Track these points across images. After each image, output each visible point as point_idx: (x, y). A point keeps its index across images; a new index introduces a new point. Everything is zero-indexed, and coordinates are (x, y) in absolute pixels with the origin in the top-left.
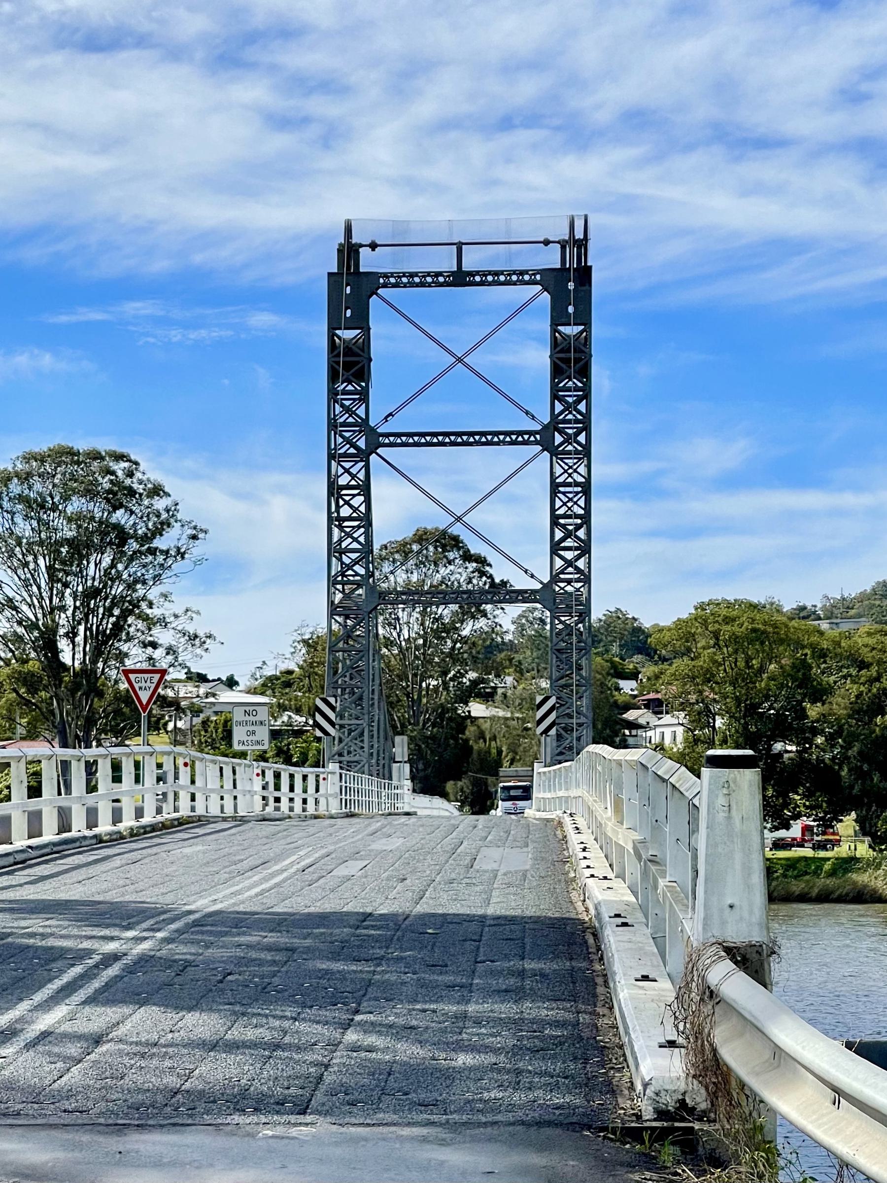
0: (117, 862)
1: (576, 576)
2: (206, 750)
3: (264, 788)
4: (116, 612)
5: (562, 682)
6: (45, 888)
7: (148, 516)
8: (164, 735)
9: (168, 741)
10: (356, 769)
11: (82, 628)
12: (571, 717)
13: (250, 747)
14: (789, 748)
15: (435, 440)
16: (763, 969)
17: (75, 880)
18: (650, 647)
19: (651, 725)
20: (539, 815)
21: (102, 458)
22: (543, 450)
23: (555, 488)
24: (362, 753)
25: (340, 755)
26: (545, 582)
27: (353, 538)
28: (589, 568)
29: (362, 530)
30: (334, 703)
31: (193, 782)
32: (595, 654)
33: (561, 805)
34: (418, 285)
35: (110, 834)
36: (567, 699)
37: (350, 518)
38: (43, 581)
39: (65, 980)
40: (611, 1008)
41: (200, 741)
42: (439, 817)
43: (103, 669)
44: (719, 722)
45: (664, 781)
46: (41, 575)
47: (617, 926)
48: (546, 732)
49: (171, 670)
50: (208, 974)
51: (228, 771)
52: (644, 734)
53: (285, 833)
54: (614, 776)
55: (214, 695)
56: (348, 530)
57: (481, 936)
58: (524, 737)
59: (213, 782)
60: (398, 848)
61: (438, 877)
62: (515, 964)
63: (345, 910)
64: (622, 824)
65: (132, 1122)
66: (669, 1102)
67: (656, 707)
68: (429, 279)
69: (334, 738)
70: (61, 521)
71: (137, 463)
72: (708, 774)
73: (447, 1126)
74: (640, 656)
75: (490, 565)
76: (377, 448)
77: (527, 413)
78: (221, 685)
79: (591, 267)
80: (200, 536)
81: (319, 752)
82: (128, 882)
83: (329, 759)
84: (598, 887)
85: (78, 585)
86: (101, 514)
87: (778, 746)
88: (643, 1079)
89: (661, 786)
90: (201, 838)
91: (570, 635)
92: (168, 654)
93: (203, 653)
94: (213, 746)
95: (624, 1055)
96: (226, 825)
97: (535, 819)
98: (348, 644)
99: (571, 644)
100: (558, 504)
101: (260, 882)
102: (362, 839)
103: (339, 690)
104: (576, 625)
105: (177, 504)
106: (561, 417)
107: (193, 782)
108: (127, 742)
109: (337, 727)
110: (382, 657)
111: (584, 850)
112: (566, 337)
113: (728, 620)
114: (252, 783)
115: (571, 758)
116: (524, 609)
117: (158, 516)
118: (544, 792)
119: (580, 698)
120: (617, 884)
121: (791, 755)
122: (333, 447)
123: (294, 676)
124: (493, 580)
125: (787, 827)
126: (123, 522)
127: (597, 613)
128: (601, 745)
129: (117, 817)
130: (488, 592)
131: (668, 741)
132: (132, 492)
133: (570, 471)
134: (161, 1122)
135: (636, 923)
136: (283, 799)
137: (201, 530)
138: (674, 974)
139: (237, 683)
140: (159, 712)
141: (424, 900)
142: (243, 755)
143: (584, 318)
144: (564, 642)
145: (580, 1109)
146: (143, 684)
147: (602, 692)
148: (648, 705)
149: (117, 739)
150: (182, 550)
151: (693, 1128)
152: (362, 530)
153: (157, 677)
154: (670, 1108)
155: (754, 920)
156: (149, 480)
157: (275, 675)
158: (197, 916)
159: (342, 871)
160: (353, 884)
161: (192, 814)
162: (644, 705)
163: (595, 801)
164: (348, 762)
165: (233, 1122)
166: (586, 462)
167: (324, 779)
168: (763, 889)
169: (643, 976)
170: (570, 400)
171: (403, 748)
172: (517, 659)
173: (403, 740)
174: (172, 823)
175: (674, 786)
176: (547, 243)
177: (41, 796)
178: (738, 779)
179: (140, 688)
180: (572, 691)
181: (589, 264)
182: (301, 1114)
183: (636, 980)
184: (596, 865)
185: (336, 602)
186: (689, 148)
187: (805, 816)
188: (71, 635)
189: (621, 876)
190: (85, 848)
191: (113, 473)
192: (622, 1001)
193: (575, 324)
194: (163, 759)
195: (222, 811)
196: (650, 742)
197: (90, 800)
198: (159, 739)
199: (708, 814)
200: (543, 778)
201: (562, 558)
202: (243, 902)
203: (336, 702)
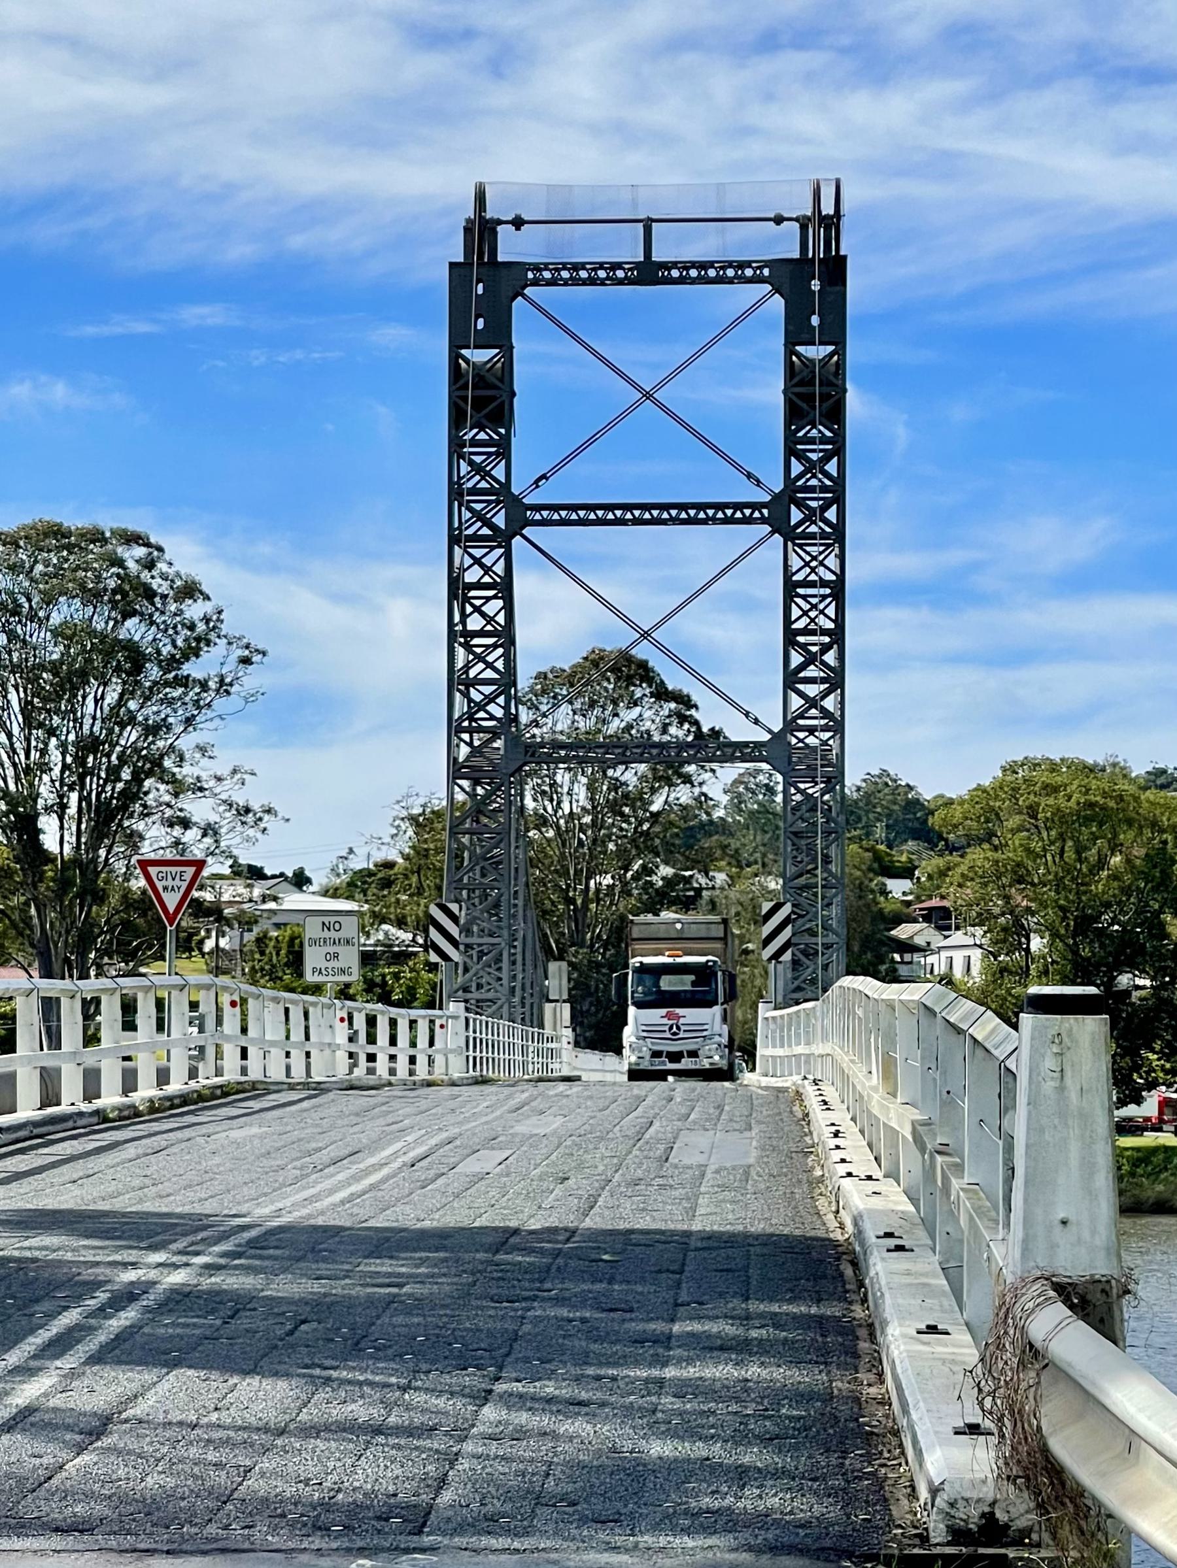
0: (131, 1150)
1: (823, 722)
2: (262, 981)
3: (351, 1040)
4: (126, 774)
5: (802, 881)
6: (22, 1191)
7: (175, 627)
8: (199, 959)
9: (205, 967)
10: (490, 1011)
11: (74, 797)
12: (815, 935)
13: (330, 978)
14: (1140, 982)
15: (610, 516)
16: (1112, 1317)
17: (67, 1178)
18: (932, 830)
19: (933, 946)
20: (766, 1081)
21: (104, 541)
22: (773, 533)
23: (791, 588)
24: (499, 988)
25: (466, 990)
26: (776, 730)
27: (486, 662)
28: (842, 709)
29: (500, 651)
30: (457, 912)
31: (244, 1030)
32: (849, 839)
33: (799, 1067)
34: (584, 283)
35: (120, 1110)
36: (808, 907)
37: (482, 633)
38: (15, 725)
39: (55, 1331)
40: (880, 1376)
41: (253, 968)
42: (614, 1084)
43: (107, 859)
44: (1037, 944)
45: (959, 1031)
46: (13, 717)
47: (889, 1251)
48: (776, 956)
49: (210, 860)
50: (270, 1322)
51: (296, 1015)
52: (922, 960)
53: (384, 1108)
54: (883, 1024)
55: (275, 899)
56: (479, 650)
57: (683, 1265)
58: (743, 965)
59: (274, 1032)
60: (555, 1131)
61: (617, 1175)
62: (736, 1304)
63: (476, 1224)
64: (895, 1096)
65: (159, 1546)
66: (972, 1516)
67: (941, 919)
68: (602, 274)
69: (457, 964)
70: (42, 635)
71: (160, 549)
72: (1031, 1021)
73: (637, 1553)
74: (915, 843)
75: (696, 707)
76: (523, 528)
77: (749, 476)
78: (284, 883)
79: (845, 257)
80: (254, 659)
81: (434, 988)
82: (147, 1181)
83: (449, 997)
84: (859, 1192)
85: (68, 732)
86: (103, 624)
87: (1124, 980)
88: (930, 1483)
89: (953, 1038)
90: (256, 1116)
91: (813, 809)
92: (204, 835)
93: (259, 835)
94: (274, 978)
95: (901, 1445)
96: (294, 1096)
97: (760, 1087)
98: (478, 822)
99: (815, 824)
100: (795, 612)
101: (348, 1182)
102: (501, 1117)
103: (464, 893)
104: (822, 795)
105: (220, 613)
106: (799, 483)
107: (244, 1030)
108: (143, 970)
109: (462, 947)
110: (531, 842)
111: (836, 1135)
112: (808, 363)
113: (1051, 789)
114: (333, 1033)
115: (814, 996)
116: (742, 771)
117: (192, 627)
118: (774, 1046)
119: (829, 905)
120: (888, 1187)
121: (1143, 993)
122: (456, 525)
123: (396, 870)
124: (699, 728)
125: (1138, 1101)
126: (137, 638)
127: (853, 778)
128: (862, 978)
129: (129, 1083)
130: (690, 745)
131: (958, 973)
132: (149, 594)
133: (814, 564)
134: (203, 1547)
135: (917, 1246)
136: (380, 1057)
137: (257, 650)
138: (975, 1322)
139: (308, 881)
140: (191, 923)
141: (596, 1210)
142: (317, 989)
143: (835, 334)
144: (804, 821)
145: (836, 1528)
146: (170, 883)
147: (860, 897)
148: (929, 916)
149: (127, 964)
150: (228, 680)
151: (1006, 1555)
152: (500, 651)
153: (190, 871)
154: (971, 1526)
155: (1098, 1242)
156: (178, 575)
157: (368, 869)
158: (254, 1233)
159: (471, 1166)
160: (488, 1186)
161: (243, 1079)
162: (922, 916)
163: (852, 1061)
164: (478, 1001)
165: (312, 1547)
166: (837, 551)
167: (442, 1026)
168: (1112, 1194)
169: (928, 1327)
170: (814, 456)
171: (560, 980)
172: (733, 846)
173: (560, 967)
174: (212, 1093)
175: (975, 1040)
176: (779, 220)
177: (15, 1052)
178: (1075, 1029)
179: (165, 888)
180: (815, 895)
181: (842, 253)
182: (415, 1534)
183: (918, 1332)
184: (855, 1158)
185: (461, 760)
186: (1042, 81)
187: (1163, 1084)
188: (61, 808)
189: (892, 1174)
190: (82, 1131)
191: (120, 563)
192: (897, 1362)
193: (821, 343)
194: (201, 996)
195: (288, 1075)
196: (932, 972)
197: (90, 1057)
198: (192, 965)
199: (1030, 1084)
200: (772, 1026)
201: (801, 694)
202: (322, 1213)
203: (460, 910)
